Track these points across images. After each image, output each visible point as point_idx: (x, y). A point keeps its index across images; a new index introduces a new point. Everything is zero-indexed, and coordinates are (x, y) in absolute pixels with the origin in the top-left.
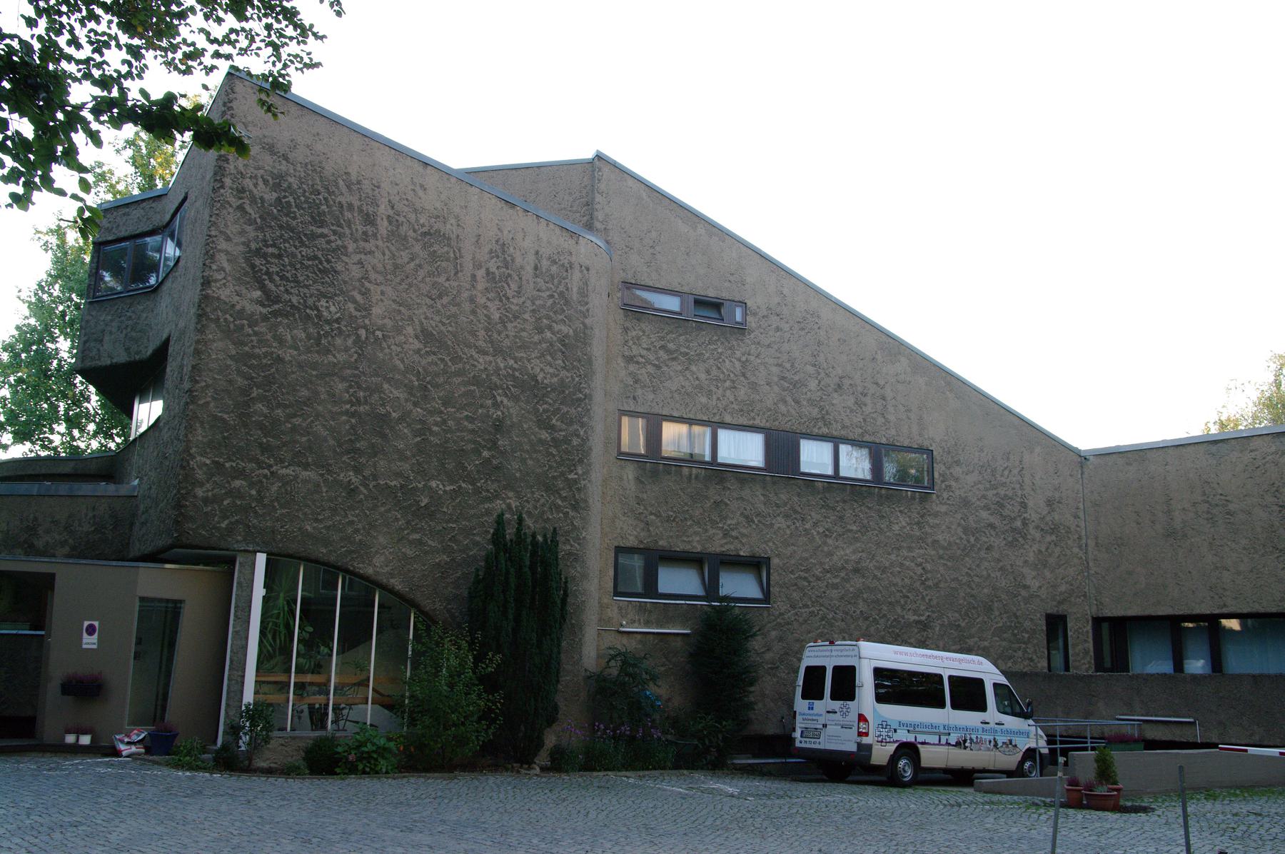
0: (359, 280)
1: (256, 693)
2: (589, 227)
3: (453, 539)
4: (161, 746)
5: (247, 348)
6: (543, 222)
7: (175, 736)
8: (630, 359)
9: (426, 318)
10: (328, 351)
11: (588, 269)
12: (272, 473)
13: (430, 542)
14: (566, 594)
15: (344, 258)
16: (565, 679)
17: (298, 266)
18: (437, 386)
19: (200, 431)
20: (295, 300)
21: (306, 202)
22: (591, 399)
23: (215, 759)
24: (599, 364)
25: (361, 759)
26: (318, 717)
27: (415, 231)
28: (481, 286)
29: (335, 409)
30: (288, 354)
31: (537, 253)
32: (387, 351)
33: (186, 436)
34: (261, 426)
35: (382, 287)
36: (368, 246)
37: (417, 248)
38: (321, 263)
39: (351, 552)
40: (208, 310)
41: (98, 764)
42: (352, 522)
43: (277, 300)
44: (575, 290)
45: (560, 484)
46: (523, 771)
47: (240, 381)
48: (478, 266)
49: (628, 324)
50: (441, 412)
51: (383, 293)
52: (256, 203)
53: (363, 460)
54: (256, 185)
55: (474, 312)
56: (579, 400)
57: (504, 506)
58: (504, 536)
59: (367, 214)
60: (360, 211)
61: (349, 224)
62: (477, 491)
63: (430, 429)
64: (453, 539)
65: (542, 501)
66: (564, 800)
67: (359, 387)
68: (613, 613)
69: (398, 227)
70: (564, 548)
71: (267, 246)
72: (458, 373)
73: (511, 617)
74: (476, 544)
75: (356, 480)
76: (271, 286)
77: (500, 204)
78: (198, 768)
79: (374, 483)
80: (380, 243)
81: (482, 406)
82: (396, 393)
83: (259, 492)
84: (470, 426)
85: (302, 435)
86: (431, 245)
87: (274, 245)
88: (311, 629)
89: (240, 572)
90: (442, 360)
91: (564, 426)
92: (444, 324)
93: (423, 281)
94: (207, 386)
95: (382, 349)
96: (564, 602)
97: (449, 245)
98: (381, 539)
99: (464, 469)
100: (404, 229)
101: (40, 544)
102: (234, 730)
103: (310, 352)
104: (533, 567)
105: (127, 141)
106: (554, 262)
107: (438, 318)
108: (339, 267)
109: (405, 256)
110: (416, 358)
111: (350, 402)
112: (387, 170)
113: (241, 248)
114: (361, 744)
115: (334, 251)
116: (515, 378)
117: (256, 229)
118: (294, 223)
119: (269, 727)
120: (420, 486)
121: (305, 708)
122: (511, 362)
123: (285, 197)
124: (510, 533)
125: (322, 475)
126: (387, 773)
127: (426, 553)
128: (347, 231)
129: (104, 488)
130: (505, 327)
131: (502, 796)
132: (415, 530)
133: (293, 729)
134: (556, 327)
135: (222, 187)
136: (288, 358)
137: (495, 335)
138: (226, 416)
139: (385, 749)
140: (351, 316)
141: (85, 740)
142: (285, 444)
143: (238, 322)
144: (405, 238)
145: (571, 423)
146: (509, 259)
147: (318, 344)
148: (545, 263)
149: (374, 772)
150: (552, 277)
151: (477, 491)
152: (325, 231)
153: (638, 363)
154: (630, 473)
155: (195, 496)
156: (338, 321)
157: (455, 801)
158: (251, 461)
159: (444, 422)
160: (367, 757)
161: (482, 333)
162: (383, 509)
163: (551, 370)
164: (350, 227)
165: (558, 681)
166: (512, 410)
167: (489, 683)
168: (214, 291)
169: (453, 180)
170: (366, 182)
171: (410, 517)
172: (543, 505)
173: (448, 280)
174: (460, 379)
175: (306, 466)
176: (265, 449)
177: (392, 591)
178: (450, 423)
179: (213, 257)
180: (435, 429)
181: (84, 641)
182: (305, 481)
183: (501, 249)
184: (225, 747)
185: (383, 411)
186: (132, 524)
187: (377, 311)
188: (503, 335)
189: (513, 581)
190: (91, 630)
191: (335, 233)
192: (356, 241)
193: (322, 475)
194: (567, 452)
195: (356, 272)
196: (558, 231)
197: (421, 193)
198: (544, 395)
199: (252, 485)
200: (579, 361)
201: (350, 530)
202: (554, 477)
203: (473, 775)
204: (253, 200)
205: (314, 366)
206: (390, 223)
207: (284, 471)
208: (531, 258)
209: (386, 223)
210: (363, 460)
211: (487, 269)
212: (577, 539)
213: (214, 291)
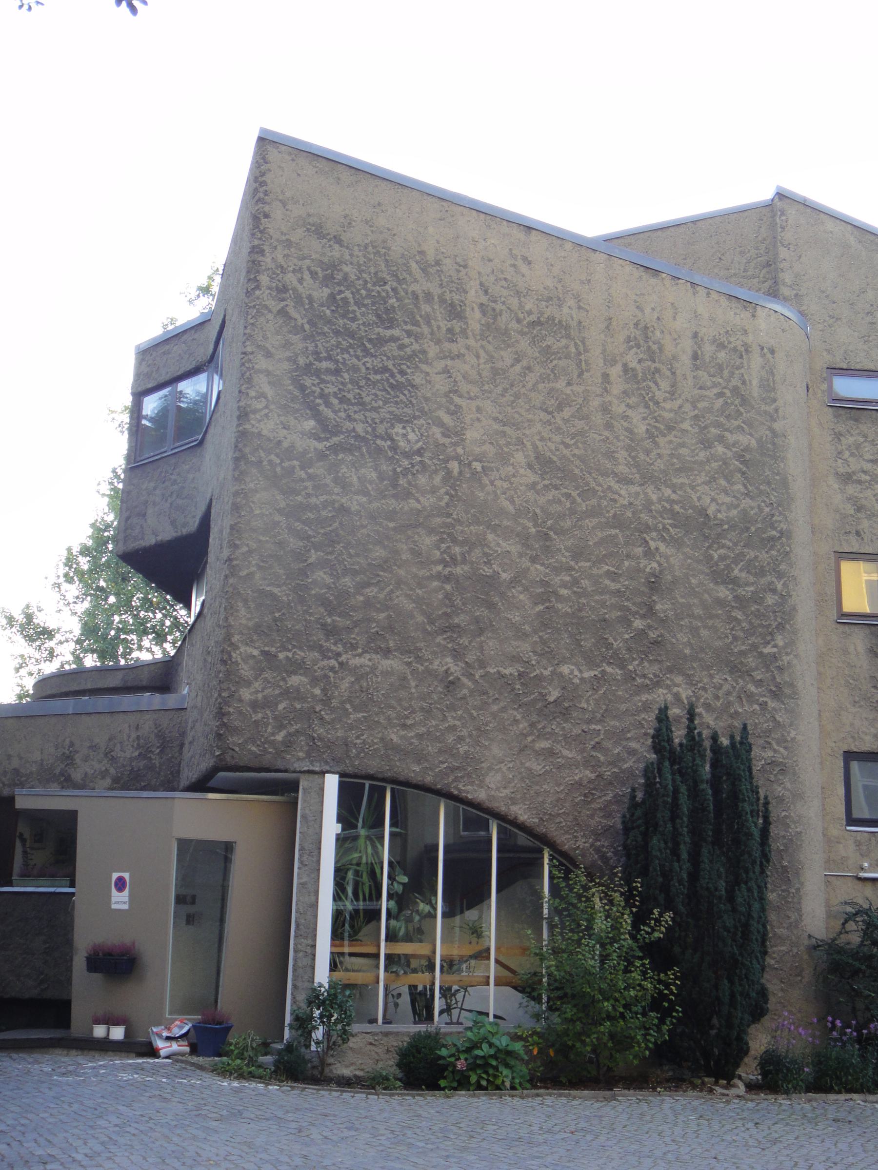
0: (446, 395)
1: (334, 966)
2: (774, 293)
3: (597, 746)
4: (209, 1041)
5: (299, 498)
6: (702, 292)
7: (228, 1029)
8: (847, 478)
9: (542, 439)
10: (408, 495)
11: (772, 352)
12: (341, 664)
13: (566, 752)
14: (767, 822)
15: (424, 367)
16: (777, 951)
17: (363, 383)
18: (561, 532)
19: (243, 612)
20: (360, 428)
21: (368, 296)
22: (789, 538)
23: (277, 1064)
24: (799, 486)
25: (473, 1067)
26: (421, 1005)
27: (519, 321)
28: (617, 388)
29: (422, 573)
30: (355, 502)
31: (695, 335)
32: (490, 488)
33: (226, 619)
34: (324, 602)
35: (478, 402)
36: (454, 348)
37: (524, 344)
38: (392, 375)
39: (453, 769)
40: (247, 450)
41: (124, 1068)
42: (453, 728)
43: (336, 431)
44: (755, 382)
45: (751, 661)
46: (719, 1090)
47: (294, 543)
48: (610, 361)
49: (841, 428)
50: (571, 569)
51: (479, 410)
52: (303, 305)
53: (464, 641)
54: (301, 281)
55: (609, 426)
56: (772, 539)
57: (669, 697)
58: (670, 740)
59: (452, 305)
60: (442, 301)
61: (428, 319)
62: (630, 677)
63: (555, 593)
64: (597, 746)
65: (726, 687)
66: (775, 1142)
67: (454, 541)
68: (847, 850)
69: (495, 318)
70: (760, 756)
71: (320, 360)
72: (592, 513)
73: (685, 856)
74: (632, 752)
75: (456, 669)
76: (328, 412)
77: (638, 273)
78: (251, 1076)
79: (481, 672)
80: (471, 342)
81: (628, 556)
82: (505, 545)
83: (324, 691)
84: (613, 586)
85: (379, 611)
86: (543, 339)
87: (329, 358)
88: (405, 879)
89: (304, 801)
90: (568, 496)
91: (752, 579)
92: (567, 446)
93: (534, 388)
94: (250, 552)
95: (483, 487)
96: (765, 832)
97: (568, 336)
98: (497, 751)
99: (609, 646)
100: (503, 320)
101: (77, 776)
102: (303, 1023)
103: (384, 497)
104: (715, 782)
105: (200, 289)
106: (722, 346)
107: (557, 438)
108: (418, 379)
109: (507, 356)
110: (531, 495)
111: (442, 561)
112: (475, 242)
113: (286, 366)
114: (476, 1045)
115: (409, 358)
116: (674, 515)
117: (305, 339)
118: (354, 326)
119: (346, 1019)
120: (546, 673)
121: (405, 990)
122: (668, 492)
123: (341, 292)
124: (679, 735)
125: (409, 664)
126: (513, 1088)
127: (559, 767)
128: (426, 330)
129: (155, 700)
130: (656, 444)
131: (678, 1131)
132: (541, 736)
133: (386, 1021)
134: (731, 438)
135: (258, 287)
136: (355, 507)
137: (642, 456)
138: (276, 590)
139: (509, 1053)
140: (437, 445)
141: (118, 1033)
142: (356, 624)
143: (286, 464)
144: (506, 332)
145: (762, 573)
146: (655, 347)
147: (395, 485)
148: (708, 349)
149: (493, 1086)
150: (720, 368)
151: (630, 677)
152: (396, 332)
153: (860, 482)
154: (859, 641)
155: (240, 700)
156: (420, 452)
157: (602, 1138)
158: (311, 648)
159: (576, 582)
160: (482, 1065)
161: (622, 455)
162: (495, 708)
163: (728, 500)
164: (428, 323)
165: (765, 953)
166: (673, 559)
167: (659, 955)
168: (252, 425)
169: (568, 246)
170: (447, 261)
171: (534, 718)
172: (728, 693)
173: (569, 384)
174: (595, 521)
175: (387, 653)
176: (331, 632)
177: (514, 823)
178: (585, 583)
179: (250, 380)
180: (564, 592)
181: (113, 899)
182: (386, 674)
183: (643, 337)
184: (289, 1048)
185: (488, 571)
186: (182, 745)
187: (471, 435)
188: (653, 455)
189: (683, 799)
190: (121, 884)
191: (409, 334)
192: (438, 342)
193: (409, 664)
194: (758, 615)
195: (441, 384)
196: (724, 301)
197: (524, 269)
198: (719, 536)
199: (315, 681)
200: (769, 483)
201: (450, 739)
202: (742, 653)
203: (640, 1094)
204: (298, 300)
205: (391, 515)
206: (484, 313)
207: (357, 661)
208: (687, 344)
209: (477, 314)
210: (464, 641)
211: (625, 365)
212: (783, 741)
213: (252, 425)
